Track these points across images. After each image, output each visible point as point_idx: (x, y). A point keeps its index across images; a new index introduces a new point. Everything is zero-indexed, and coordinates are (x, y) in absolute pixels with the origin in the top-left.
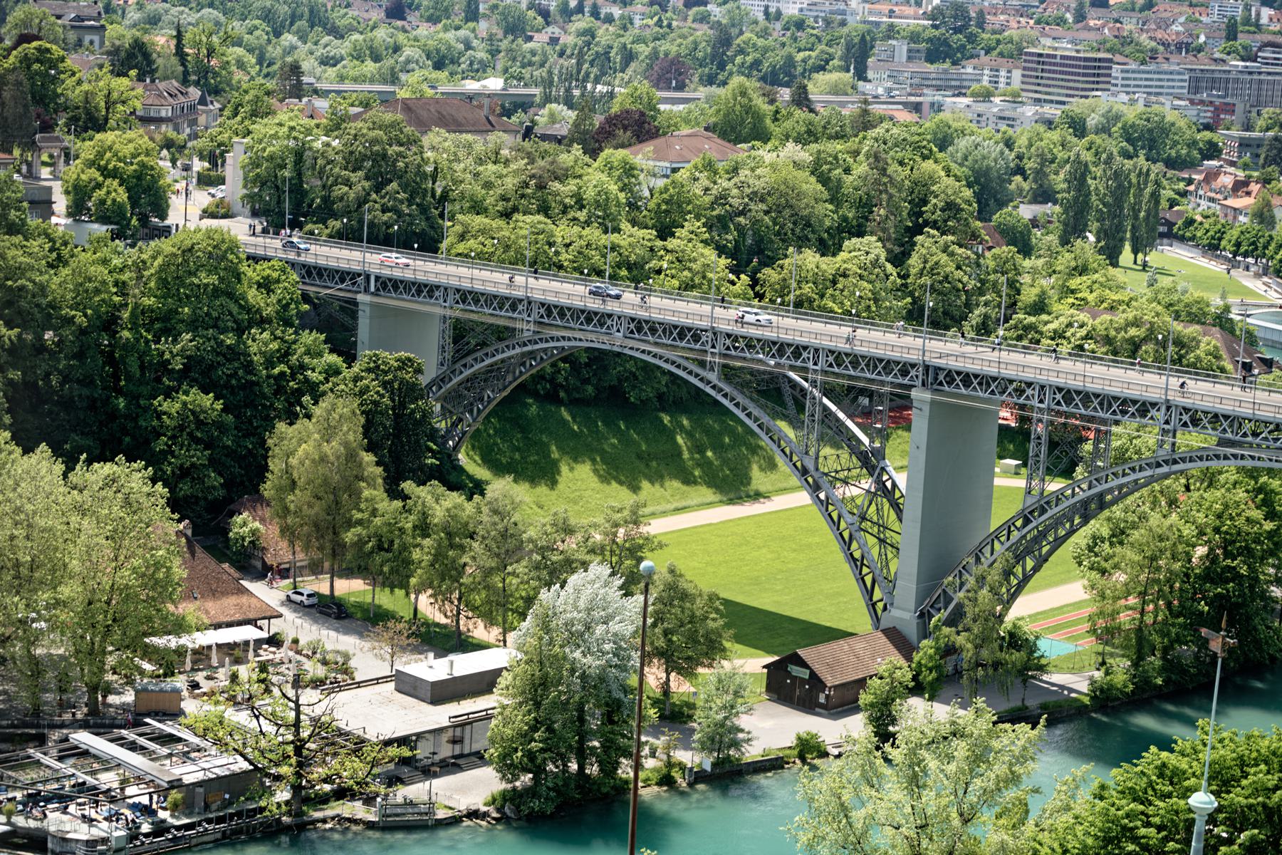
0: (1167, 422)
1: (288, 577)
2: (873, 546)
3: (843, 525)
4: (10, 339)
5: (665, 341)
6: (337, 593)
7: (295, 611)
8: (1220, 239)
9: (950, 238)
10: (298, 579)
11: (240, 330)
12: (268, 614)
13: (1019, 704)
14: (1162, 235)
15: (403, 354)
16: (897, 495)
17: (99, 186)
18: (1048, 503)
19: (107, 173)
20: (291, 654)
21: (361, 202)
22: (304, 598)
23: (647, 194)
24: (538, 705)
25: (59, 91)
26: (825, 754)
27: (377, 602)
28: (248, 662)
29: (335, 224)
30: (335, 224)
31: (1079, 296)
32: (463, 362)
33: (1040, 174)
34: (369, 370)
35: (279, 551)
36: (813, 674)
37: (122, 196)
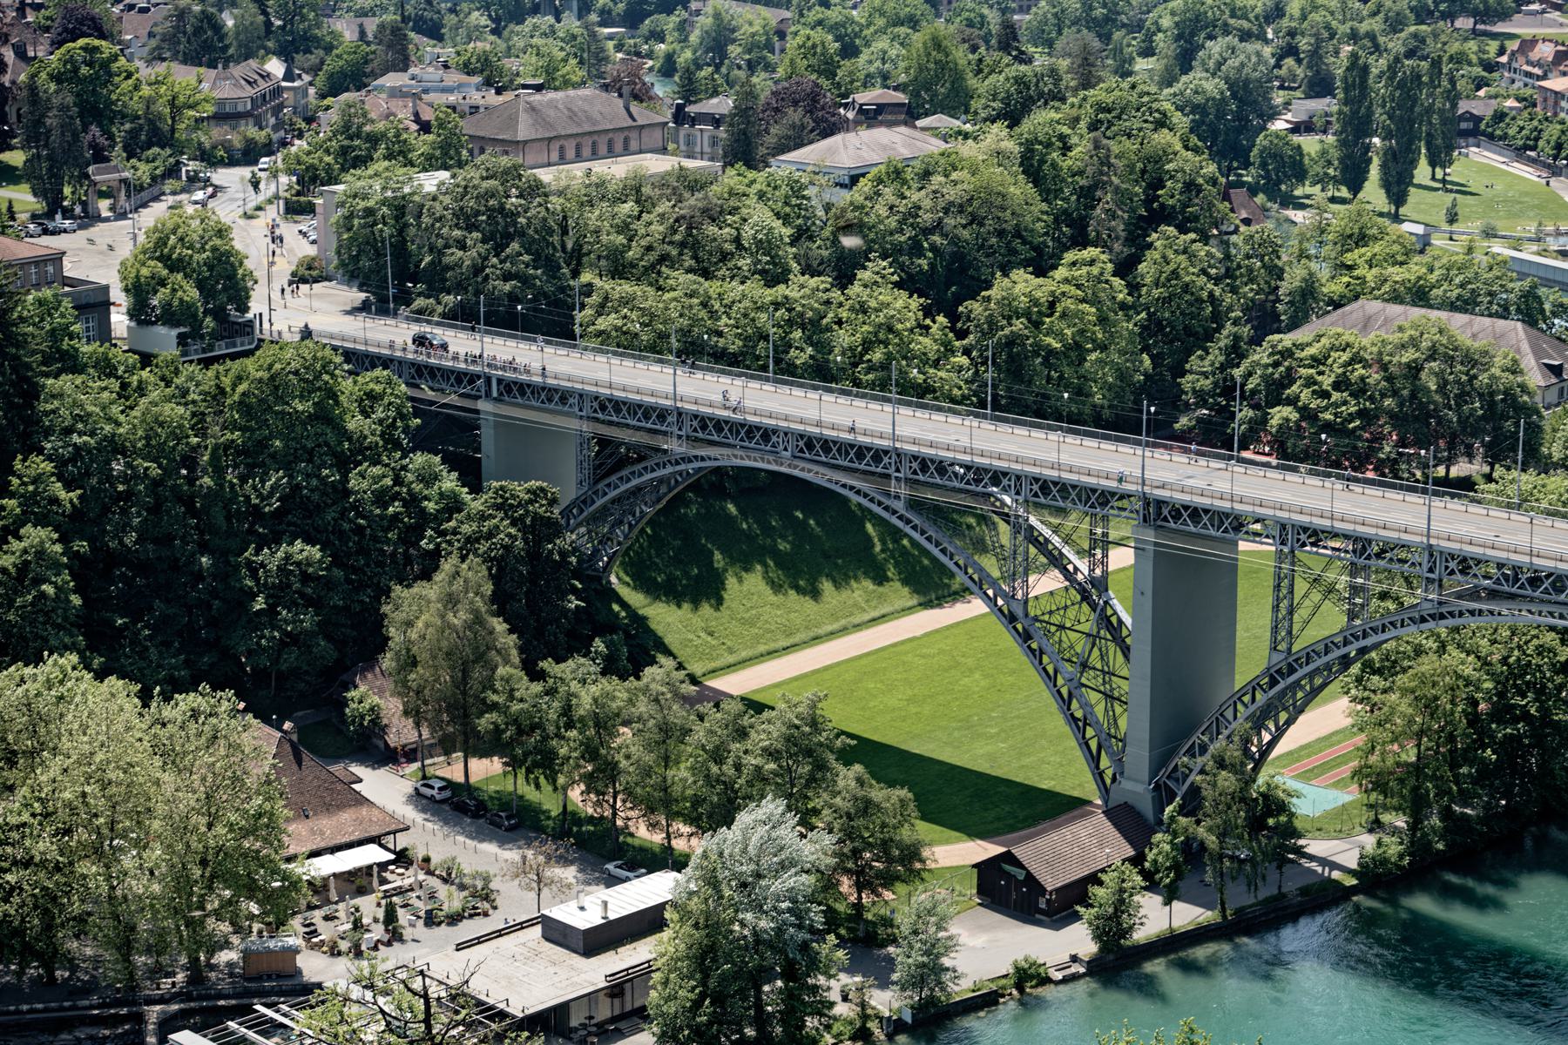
0: (1431, 570)
1: (415, 760)
2: (1098, 702)
3: (1060, 681)
4: (71, 501)
5: (840, 462)
6: (473, 780)
7: (424, 811)
8: (1537, 139)
9: (1192, 236)
10: (428, 762)
11: (344, 464)
12: (393, 827)
13: (1276, 892)
14: (1465, 134)
15: (534, 484)
16: (1124, 633)
17: (162, 283)
18: (1296, 660)
19: (174, 265)
20: (421, 876)
21: (477, 269)
22: (435, 792)
23: (820, 213)
24: (706, 976)
25: (114, 97)
26: (1046, 980)
27: (520, 792)
28: (373, 891)
29: (450, 299)
30: (450, 299)
31: (1356, 273)
32: (607, 481)
33: (1316, 54)
34: (498, 507)
35: (401, 732)
36: (1029, 876)
37: (192, 293)
